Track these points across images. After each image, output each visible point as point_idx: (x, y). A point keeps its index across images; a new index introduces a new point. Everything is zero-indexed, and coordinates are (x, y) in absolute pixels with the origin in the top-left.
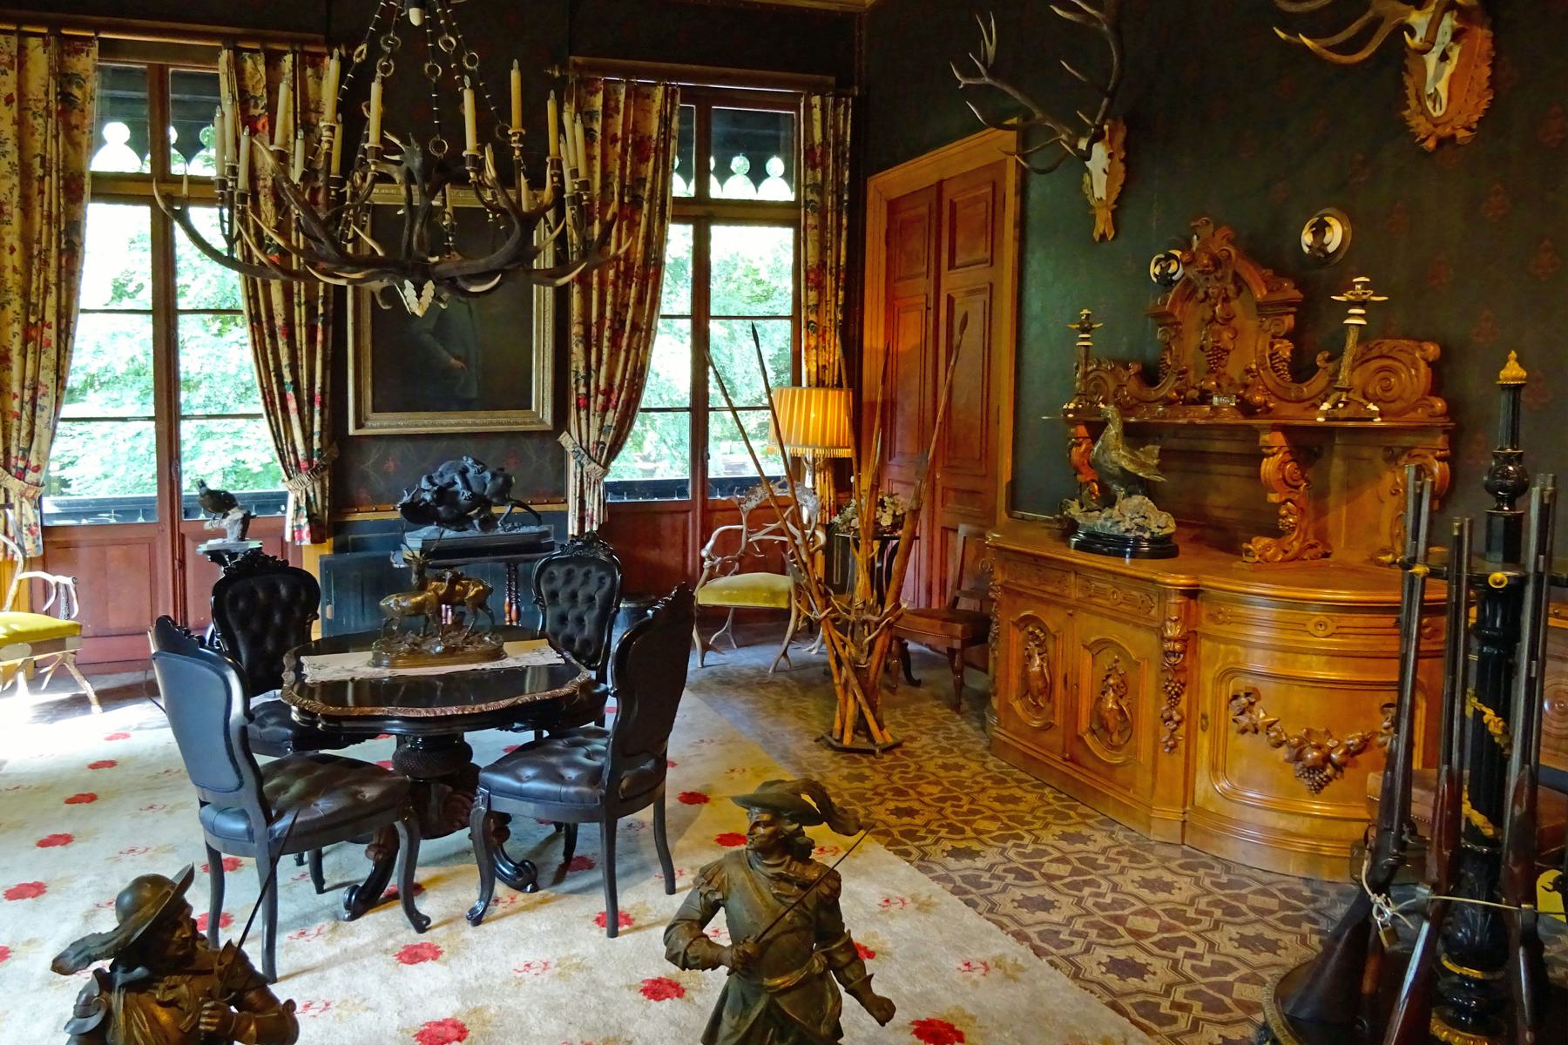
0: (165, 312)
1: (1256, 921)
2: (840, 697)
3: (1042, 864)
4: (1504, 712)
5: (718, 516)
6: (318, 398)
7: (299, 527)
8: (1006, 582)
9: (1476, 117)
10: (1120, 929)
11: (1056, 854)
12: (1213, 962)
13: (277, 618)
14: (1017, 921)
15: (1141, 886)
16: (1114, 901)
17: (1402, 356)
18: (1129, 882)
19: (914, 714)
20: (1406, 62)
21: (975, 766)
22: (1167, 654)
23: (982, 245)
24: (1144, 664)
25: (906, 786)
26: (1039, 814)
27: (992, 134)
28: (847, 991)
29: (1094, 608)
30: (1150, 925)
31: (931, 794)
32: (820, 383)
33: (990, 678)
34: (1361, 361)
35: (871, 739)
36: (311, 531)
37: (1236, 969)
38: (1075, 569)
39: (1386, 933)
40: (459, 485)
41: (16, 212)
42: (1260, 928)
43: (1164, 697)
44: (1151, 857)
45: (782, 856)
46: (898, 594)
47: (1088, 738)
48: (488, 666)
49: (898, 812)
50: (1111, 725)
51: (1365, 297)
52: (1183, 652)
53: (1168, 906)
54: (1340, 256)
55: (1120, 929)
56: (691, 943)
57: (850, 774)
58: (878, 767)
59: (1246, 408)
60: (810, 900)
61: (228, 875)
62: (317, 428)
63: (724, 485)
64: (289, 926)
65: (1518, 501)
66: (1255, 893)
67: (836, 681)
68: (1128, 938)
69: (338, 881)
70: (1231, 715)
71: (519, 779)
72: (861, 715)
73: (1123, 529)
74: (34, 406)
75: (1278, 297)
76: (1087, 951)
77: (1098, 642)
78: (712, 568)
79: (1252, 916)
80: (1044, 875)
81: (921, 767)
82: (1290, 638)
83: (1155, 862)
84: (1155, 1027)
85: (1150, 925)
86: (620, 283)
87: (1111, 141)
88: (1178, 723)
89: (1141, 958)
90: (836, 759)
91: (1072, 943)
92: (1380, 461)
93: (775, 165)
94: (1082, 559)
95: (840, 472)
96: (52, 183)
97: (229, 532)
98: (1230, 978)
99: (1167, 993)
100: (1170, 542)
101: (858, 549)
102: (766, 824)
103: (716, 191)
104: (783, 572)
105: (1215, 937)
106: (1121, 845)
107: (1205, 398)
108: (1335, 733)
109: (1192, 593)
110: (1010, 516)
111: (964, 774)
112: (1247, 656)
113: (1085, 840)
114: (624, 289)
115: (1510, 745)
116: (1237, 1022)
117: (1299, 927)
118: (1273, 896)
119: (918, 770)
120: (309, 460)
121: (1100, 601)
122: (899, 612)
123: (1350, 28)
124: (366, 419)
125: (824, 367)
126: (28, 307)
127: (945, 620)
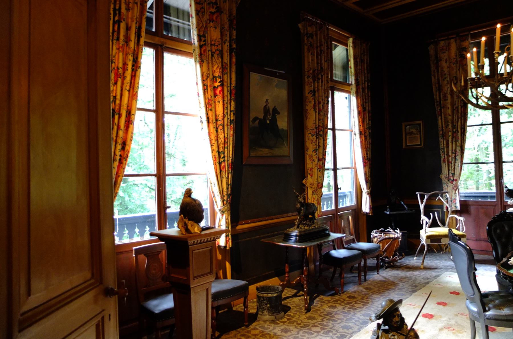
61: (490, 332)
74: (455, 159)
126: (454, 127)
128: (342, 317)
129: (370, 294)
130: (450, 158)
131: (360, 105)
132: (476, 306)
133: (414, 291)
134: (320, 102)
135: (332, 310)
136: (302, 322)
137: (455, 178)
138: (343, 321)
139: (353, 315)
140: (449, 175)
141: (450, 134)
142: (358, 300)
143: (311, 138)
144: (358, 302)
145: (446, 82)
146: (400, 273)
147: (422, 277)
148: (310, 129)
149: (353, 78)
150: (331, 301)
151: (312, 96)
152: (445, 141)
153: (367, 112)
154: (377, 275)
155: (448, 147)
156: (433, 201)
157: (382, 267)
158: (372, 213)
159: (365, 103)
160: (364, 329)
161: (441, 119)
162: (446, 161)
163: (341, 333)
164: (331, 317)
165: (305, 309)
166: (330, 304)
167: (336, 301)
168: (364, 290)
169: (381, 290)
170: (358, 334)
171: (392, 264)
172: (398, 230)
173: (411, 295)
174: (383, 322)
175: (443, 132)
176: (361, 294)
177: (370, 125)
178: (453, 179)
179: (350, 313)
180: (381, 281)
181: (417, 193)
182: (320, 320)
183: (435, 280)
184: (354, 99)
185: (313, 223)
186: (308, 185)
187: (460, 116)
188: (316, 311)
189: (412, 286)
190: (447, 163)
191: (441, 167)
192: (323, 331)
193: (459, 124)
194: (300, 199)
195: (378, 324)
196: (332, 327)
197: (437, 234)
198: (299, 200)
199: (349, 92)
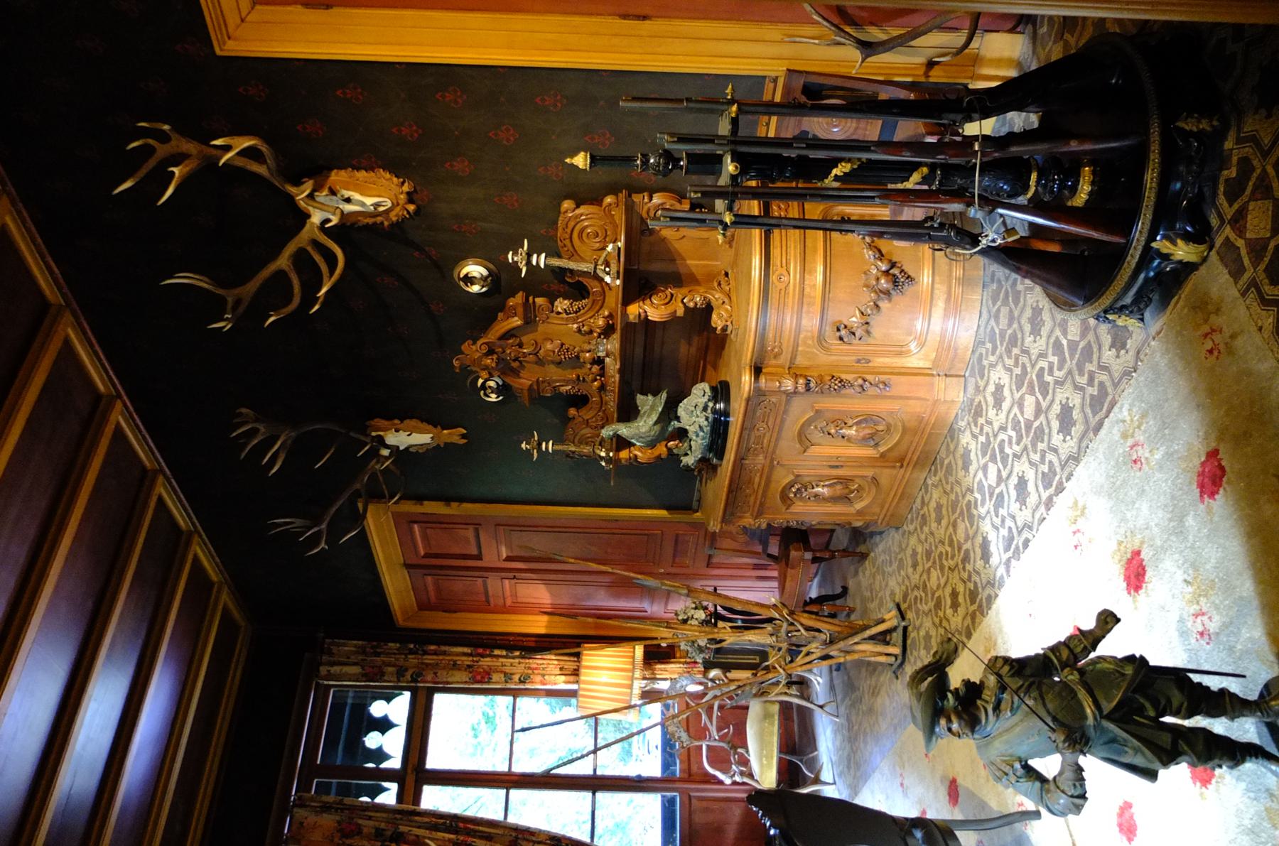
1: (1019, 323)
2: (856, 656)
3: (990, 486)
4: (835, 162)
5: (694, 768)
8: (752, 515)
9: (395, 179)
12: (1053, 355)
14: (1037, 507)
15: (1000, 408)
16: (1014, 429)
17: (572, 224)
19: (872, 593)
20: (349, 224)
22: (808, 389)
23: (462, 532)
24: (817, 406)
25: (932, 599)
27: (370, 522)
28: (1094, 650)
29: (772, 445)
30: (1030, 401)
32: (576, 673)
33: (836, 527)
34: (574, 255)
35: (895, 629)
37: (1057, 338)
39: (1009, 237)
42: (1024, 321)
43: (844, 391)
44: (977, 400)
45: (978, 708)
46: (763, 606)
47: (882, 449)
49: (955, 605)
50: (868, 431)
51: (524, 254)
52: (805, 377)
53: (1014, 388)
54: (491, 266)
55: (1036, 424)
56: (1063, 792)
58: (917, 623)
59: (608, 331)
60: (1014, 683)
63: (666, 765)
65: (676, 156)
66: (997, 323)
67: (842, 660)
68: (1042, 418)
70: (856, 341)
72: (872, 638)
73: (706, 423)
75: (520, 310)
76: (1055, 451)
77: (800, 441)
78: (742, 774)
79: (1015, 326)
80: (998, 485)
81: (916, 586)
82: (792, 300)
83: (980, 398)
84: (1110, 398)
85: (1030, 401)
87: (386, 430)
88: (865, 381)
89: (1056, 409)
90: (912, 660)
92: (652, 239)
93: (378, 709)
95: (657, 655)
98: (1065, 342)
99: (1082, 389)
100: (717, 387)
101: (724, 641)
102: (949, 721)
103: (395, 763)
104: (747, 708)
105: (1034, 353)
106: (969, 424)
107: (599, 361)
108: (866, 268)
109: (757, 371)
110: (697, 511)
111: (919, 550)
112: (807, 331)
115: (859, 159)
116: (1097, 338)
117: (1020, 291)
118: (999, 310)
119: (918, 588)
122: (779, 605)
123: (318, 261)
125: (561, 669)
127: (787, 565)
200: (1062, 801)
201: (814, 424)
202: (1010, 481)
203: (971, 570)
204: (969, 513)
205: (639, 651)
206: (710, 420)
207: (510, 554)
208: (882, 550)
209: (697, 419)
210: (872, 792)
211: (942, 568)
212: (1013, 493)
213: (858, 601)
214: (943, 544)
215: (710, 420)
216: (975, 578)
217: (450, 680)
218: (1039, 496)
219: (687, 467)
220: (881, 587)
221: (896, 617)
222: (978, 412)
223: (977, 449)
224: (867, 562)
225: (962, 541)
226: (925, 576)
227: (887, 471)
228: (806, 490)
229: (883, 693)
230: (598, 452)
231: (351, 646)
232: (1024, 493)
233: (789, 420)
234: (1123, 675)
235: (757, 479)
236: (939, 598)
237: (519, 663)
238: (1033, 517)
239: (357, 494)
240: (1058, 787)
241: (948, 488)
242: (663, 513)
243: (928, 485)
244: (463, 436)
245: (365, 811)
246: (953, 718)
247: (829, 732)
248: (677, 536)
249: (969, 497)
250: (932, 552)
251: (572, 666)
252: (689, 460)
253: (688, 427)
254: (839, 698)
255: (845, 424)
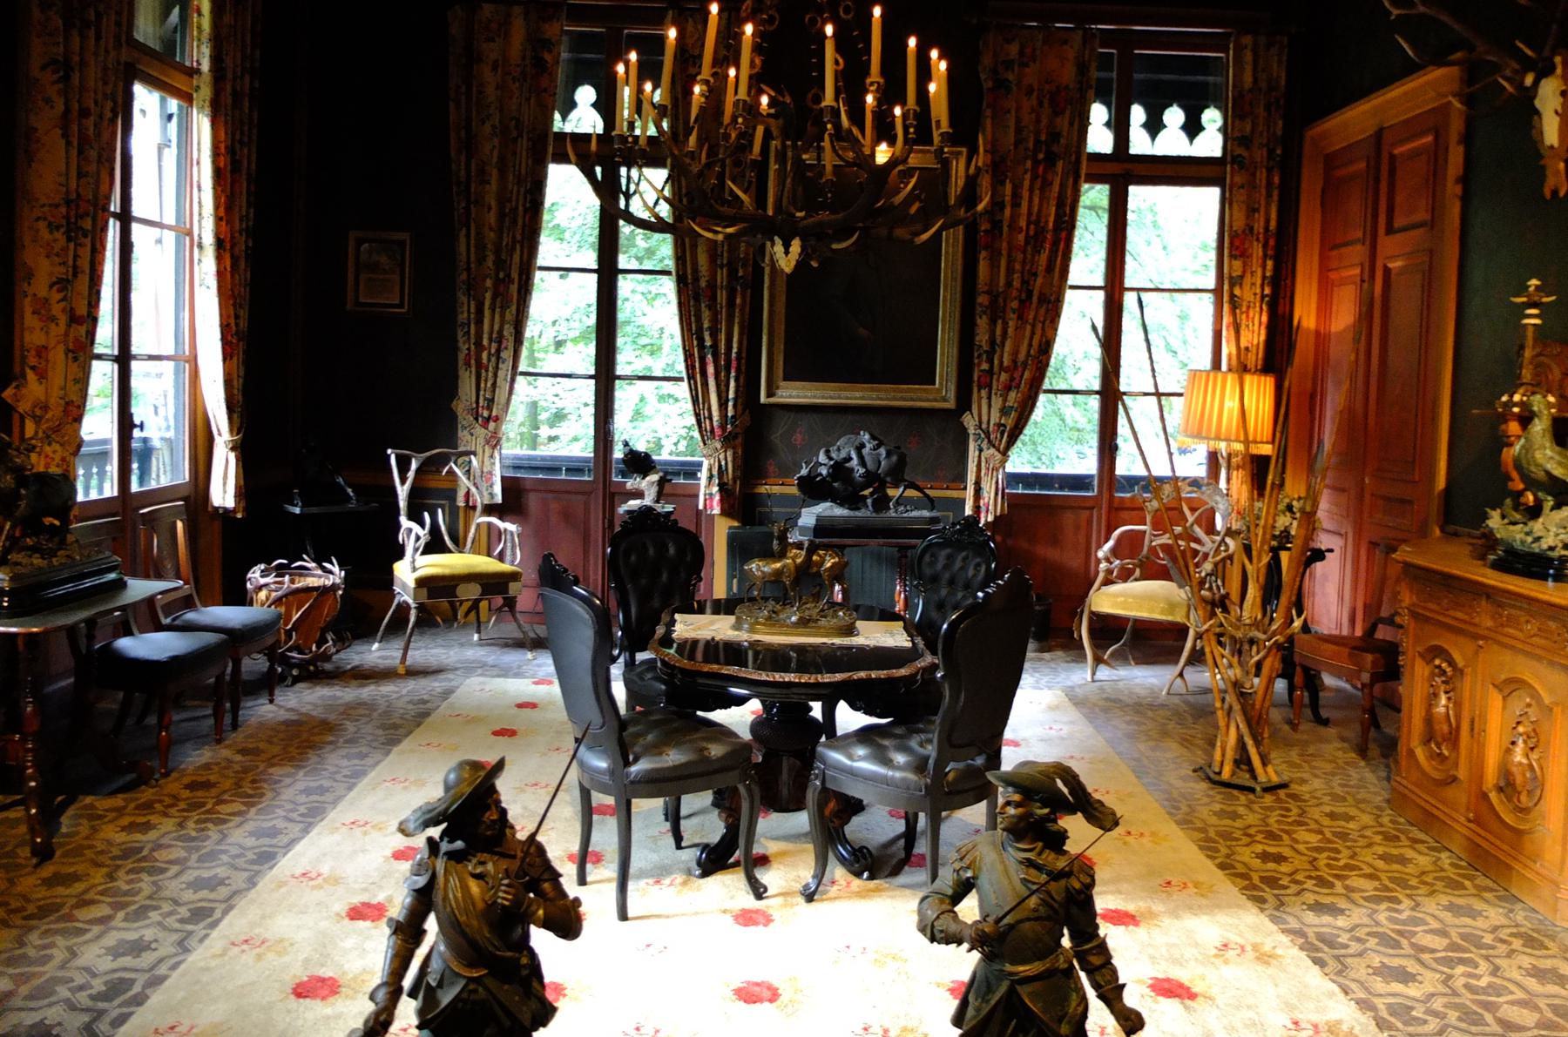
0: (608, 273)
2: (1222, 723)
3: (1415, 933)
5: (1125, 515)
6: (734, 364)
7: (711, 494)
8: (1414, 605)
10: (1488, 1017)
11: (1435, 925)
13: (665, 577)
16: (1490, 985)
18: (1514, 968)
19: (1311, 755)
21: (1367, 819)
25: (1282, 830)
26: (1428, 879)
29: (1506, 640)
31: (1307, 843)
35: (1254, 777)
36: (722, 500)
38: (1487, 593)
40: (855, 462)
41: (495, 172)
44: (1551, 944)
45: (1034, 841)
47: (1493, 796)
48: (838, 641)
49: (1265, 857)
53: (1556, 1001)
55: (1488, 1017)
56: (938, 917)
57: (1222, 810)
58: (1256, 807)
60: (1057, 888)
62: (731, 395)
63: (1132, 481)
64: (642, 874)
69: (697, 841)
71: (850, 757)
73: (1545, 546)
74: (498, 358)
78: (1110, 572)
80: (1413, 945)
81: (1304, 812)
86: (1029, 249)
90: (1211, 793)
91: (1425, 1022)
93: (1212, 118)
94: (1494, 579)
95: (1258, 469)
96: (524, 144)
97: (646, 493)
102: (1017, 805)
103: (1140, 143)
110: (1442, 531)
111: (1352, 825)
113: (1473, 914)
114: (1033, 256)
120: (723, 426)
121: (1511, 631)
124: (778, 388)
125: (1247, 349)
126: (500, 264)
128: (183, 854)
129: (261, 769)
130: (485, 355)
131: (223, 150)
132: (605, 753)
133: (393, 742)
134: (88, 109)
135: (139, 837)
136: (28, 901)
137: (494, 413)
138: (189, 864)
139: (219, 842)
140: (477, 402)
141: (489, 283)
142: (225, 792)
143: (45, 235)
144: (226, 797)
145: (487, 128)
146: (339, 694)
147: (408, 699)
148: (41, 202)
149: (206, 50)
150: (127, 811)
151: (58, 81)
152: (473, 304)
153: (244, 177)
154: (270, 707)
155: (480, 322)
156: (431, 477)
157: (282, 679)
158: (245, 510)
159: (238, 146)
160: (268, 877)
161: (468, 236)
162: (473, 362)
163: (191, 906)
164: (139, 860)
165: (34, 854)
166: (126, 821)
167: (147, 807)
168: (239, 758)
169: (291, 749)
170: (252, 894)
171: (312, 668)
172: (332, 564)
173: (388, 753)
174: (444, 834)
175: (469, 275)
176: (230, 773)
177: (251, 223)
178: (489, 415)
179: (208, 837)
180: (287, 723)
181: (389, 451)
182: (102, 880)
183: (445, 704)
184: (202, 127)
185: (63, 544)
186: (23, 407)
187: (519, 237)
188: (78, 852)
189: (384, 727)
190: (473, 369)
191: (456, 377)
192: (121, 915)
193: (516, 258)
194: (17, 457)
195: (430, 840)
196: (156, 893)
197: (447, 571)
198: (11, 460)
199: (187, 98)
200: (929, 912)
201: (1533, 703)
202: (1412, 962)
203: (1305, 886)
204: (1385, 896)
205: (1266, 449)
206: (1550, 553)
207: (1393, 272)
208: (1368, 780)
209: (1552, 534)
210: (1072, 723)
211: (1317, 849)
212: (1395, 962)
213: (1305, 737)
214: (1351, 857)
215: (1550, 553)
216: (1294, 888)
217: (1235, 206)
218: (1380, 995)
219: (1485, 517)
220: (1315, 768)
221: (1269, 781)
222: (1531, 942)
223: (1474, 928)
224: (1354, 755)
225: (1347, 882)
226: (1313, 826)
227: (1464, 800)
228: (1443, 682)
229: (1184, 751)
230: (1521, 390)
231: (1280, 73)
232: (1391, 976)
233: (1543, 670)
234: (1060, 1021)
235: (1459, 615)
236: (1281, 839)
237: (1255, 294)
238: (1354, 980)
239: (1472, 49)
240: (942, 913)
241: (1428, 879)
242: (1441, 483)
243: (1439, 852)
244: (1555, 192)
245: (1079, 116)
246: (1020, 810)
247: (1153, 681)
248: (1410, 502)
249: (1407, 903)
250: (1345, 841)
251: (1251, 363)
252: (1494, 521)
253: (1541, 520)
254: (1190, 698)
255: (1532, 749)
